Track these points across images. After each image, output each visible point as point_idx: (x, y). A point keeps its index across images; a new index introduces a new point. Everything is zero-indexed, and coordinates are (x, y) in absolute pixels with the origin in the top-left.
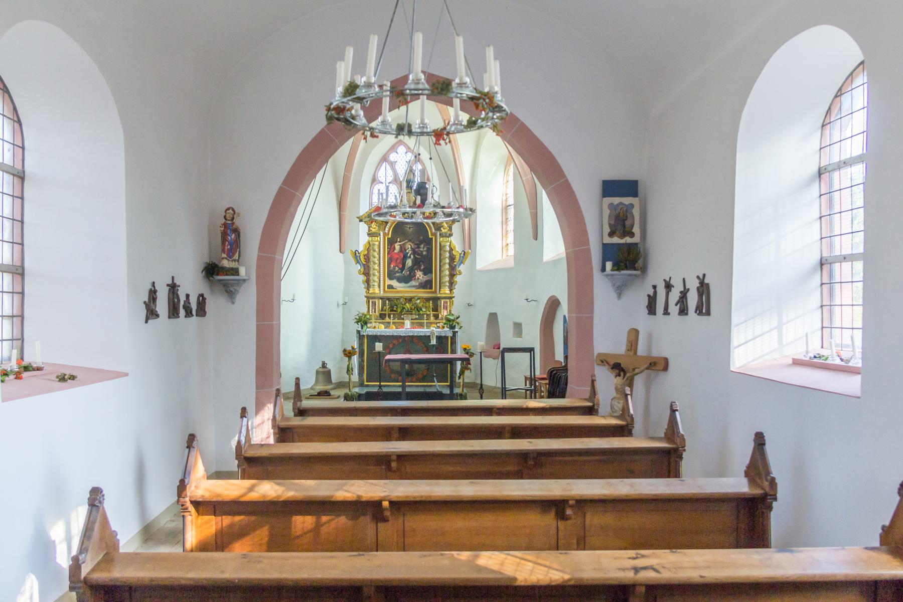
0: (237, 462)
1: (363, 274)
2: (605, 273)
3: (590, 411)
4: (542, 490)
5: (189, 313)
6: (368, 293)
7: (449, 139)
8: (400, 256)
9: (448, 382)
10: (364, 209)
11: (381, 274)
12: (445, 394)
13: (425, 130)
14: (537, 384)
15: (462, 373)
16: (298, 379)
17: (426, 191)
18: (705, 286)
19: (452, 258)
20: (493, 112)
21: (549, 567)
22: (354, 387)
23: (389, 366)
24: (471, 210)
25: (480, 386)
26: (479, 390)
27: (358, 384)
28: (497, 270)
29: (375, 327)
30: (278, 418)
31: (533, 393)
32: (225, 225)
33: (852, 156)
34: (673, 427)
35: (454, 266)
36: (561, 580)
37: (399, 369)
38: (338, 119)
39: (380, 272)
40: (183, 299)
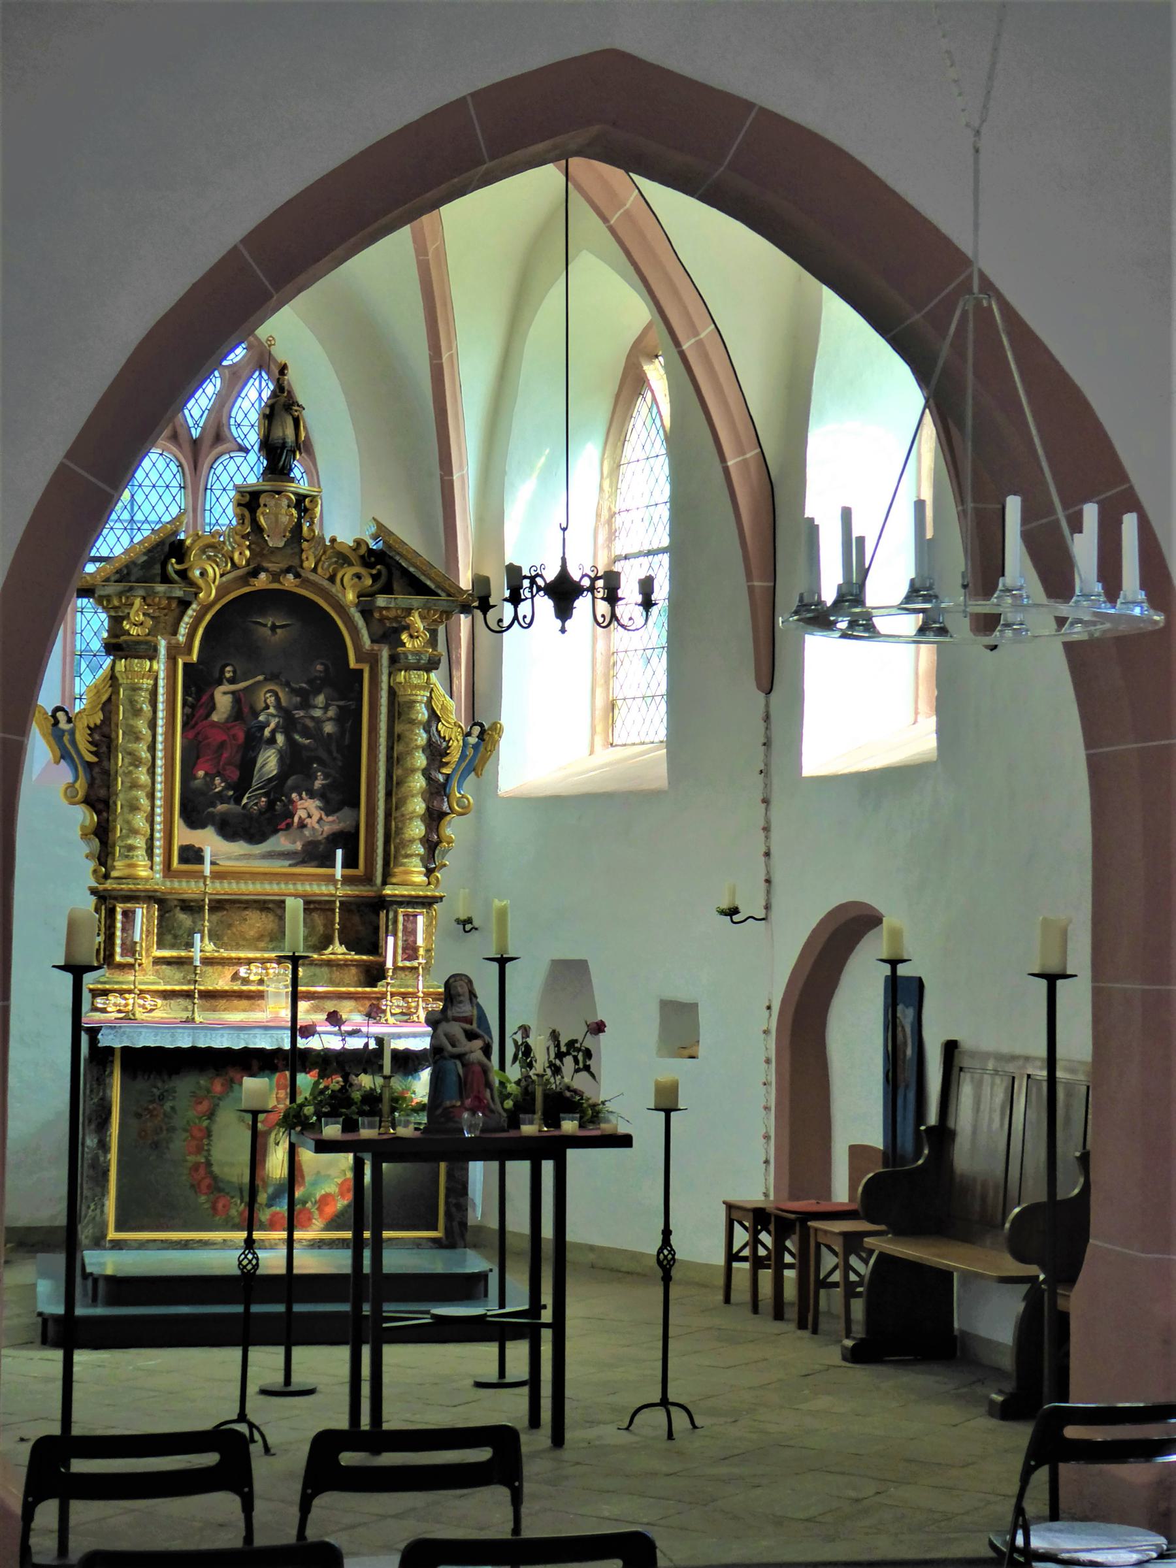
8: (234, 736)
9: (436, 1229)
19: (436, 752)
33: (140, 468)
35: (441, 778)
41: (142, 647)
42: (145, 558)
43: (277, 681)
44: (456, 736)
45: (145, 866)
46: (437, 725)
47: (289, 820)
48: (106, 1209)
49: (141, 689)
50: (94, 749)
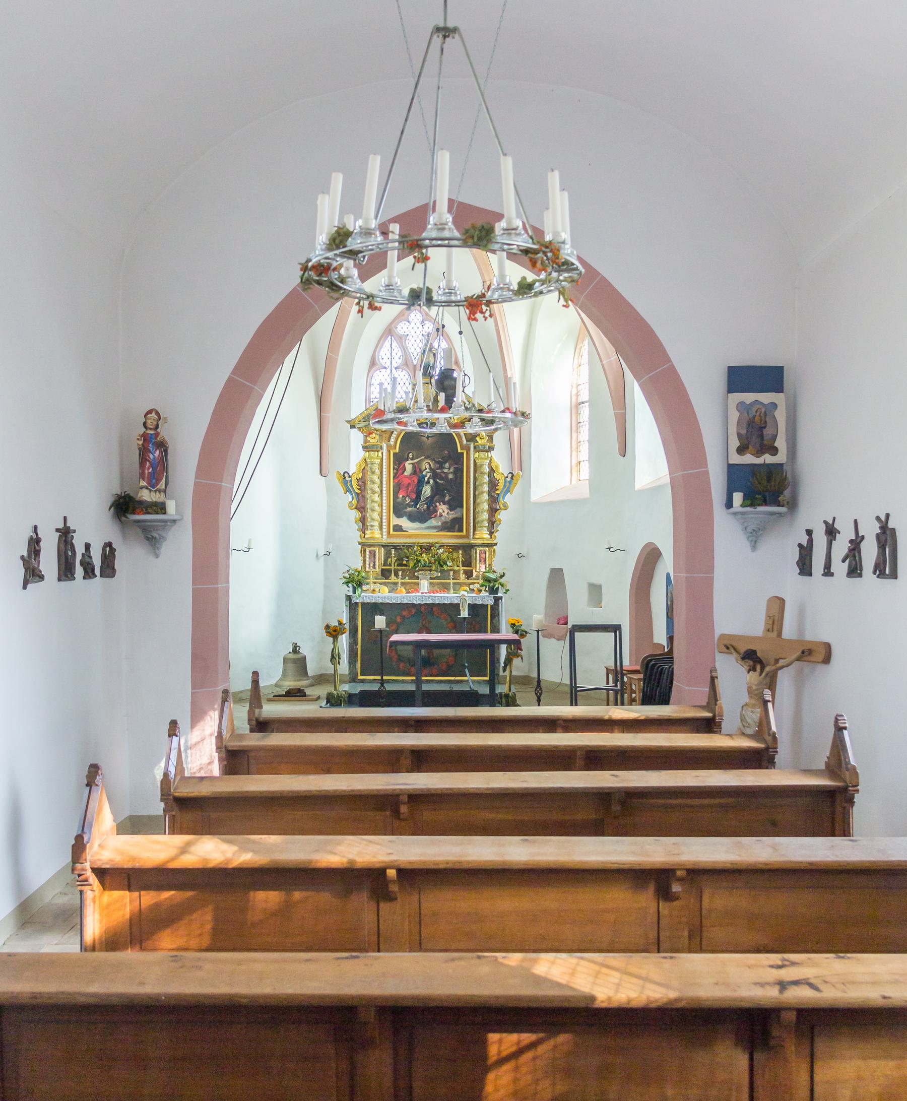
0: (162, 805)
2: (731, 510)
3: (709, 725)
4: (634, 853)
5: (89, 572)
6: (364, 537)
9: (486, 676)
10: (357, 409)
11: (384, 508)
13: (453, 298)
14: (626, 679)
15: (508, 661)
16: (256, 674)
17: (453, 383)
18: (888, 532)
19: (493, 484)
20: (559, 271)
21: (646, 979)
22: (342, 682)
23: (396, 650)
24: (523, 414)
25: (536, 684)
26: (536, 690)
28: (562, 502)
29: (374, 590)
30: (226, 735)
31: (619, 697)
32: (145, 437)
34: (839, 756)
36: (665, 1000)
37: (411, 655)
38: (319, 283)
40: (80, 550)
49: (375, 463)
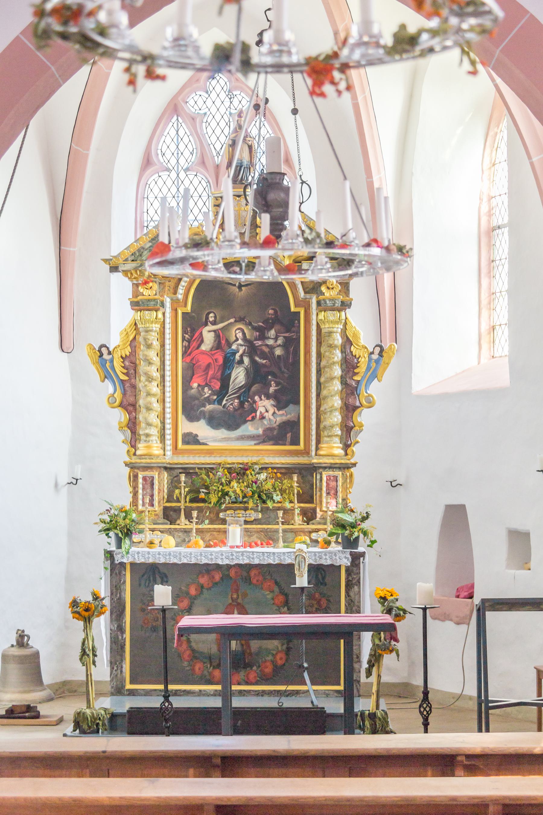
1: (121, 405)
6: (135, 454)
7: (347, 80)
9: (339, 684)
11: (168, 405)
12: (332, 716)
13: (285, 59)
22: (100, 694)
23: (189, 641)
24: (400, 249)
25: (421, 696)
27: (108, 688)
29: (151, 543)
38: (64, 36)
39: (164, 401)
41: (152, 303)
42: (150, 244)
43: (242, 322)
44: (363, 354)
45: (157, 447)
46: (350, 348)
47: (253, 414)
48: (124, 670)
50: (125, 371)
